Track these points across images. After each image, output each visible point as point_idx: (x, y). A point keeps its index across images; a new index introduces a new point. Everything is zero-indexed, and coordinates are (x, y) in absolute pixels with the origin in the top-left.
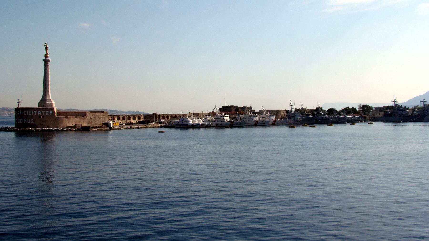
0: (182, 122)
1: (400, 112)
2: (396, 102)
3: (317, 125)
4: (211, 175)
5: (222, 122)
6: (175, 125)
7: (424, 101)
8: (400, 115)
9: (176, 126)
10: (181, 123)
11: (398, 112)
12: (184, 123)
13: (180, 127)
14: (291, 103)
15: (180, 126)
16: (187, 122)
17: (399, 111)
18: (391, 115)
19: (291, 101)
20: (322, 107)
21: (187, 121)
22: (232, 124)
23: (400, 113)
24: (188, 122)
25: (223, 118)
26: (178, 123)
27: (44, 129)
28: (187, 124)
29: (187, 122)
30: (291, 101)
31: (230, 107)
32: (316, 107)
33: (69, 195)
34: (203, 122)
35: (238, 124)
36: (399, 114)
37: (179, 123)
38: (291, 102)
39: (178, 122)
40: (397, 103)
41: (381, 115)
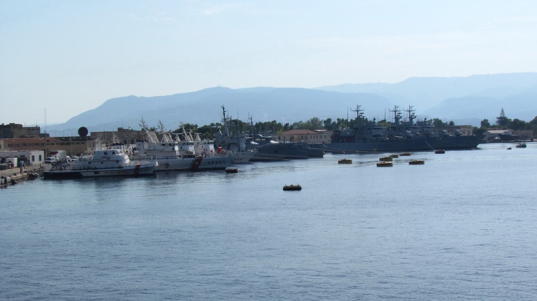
0: (102, 163)
1: (375, 132)
2: (359, 112)
3: (249, 167)
4: (328, 265)
5: (169, 160)
6: (81, 169)
7: (398, 109)
8: (375, 138)
9: (84, 174)
10: (100, 163)
11: (371, 131)
12: (109, 164)
13: (97, 175)
14: (224, 114)
15: (96, 173)
16: (117, 161)
17: (373, 130)
18: (349, 139)
19: (224, 109)
20: (40, 127)
21: (120, 159)
22: (197, 163)
23: (374, 134)
24: (121, 160)
25: (172, 150)
26: (89, 165)
27: (441, 150)
28: (120, 167)
29: (117, 161)
30: (224, 109)
31: (355, 121)
32: (524, 120)
33: (324, 288)
34: (131, 160)
35: (213, 162)
36: (374, 136)
37: (93, 165)
38: (224, 111)
39: (89, 163)
40: (363, 113)
41: (327, 138)
